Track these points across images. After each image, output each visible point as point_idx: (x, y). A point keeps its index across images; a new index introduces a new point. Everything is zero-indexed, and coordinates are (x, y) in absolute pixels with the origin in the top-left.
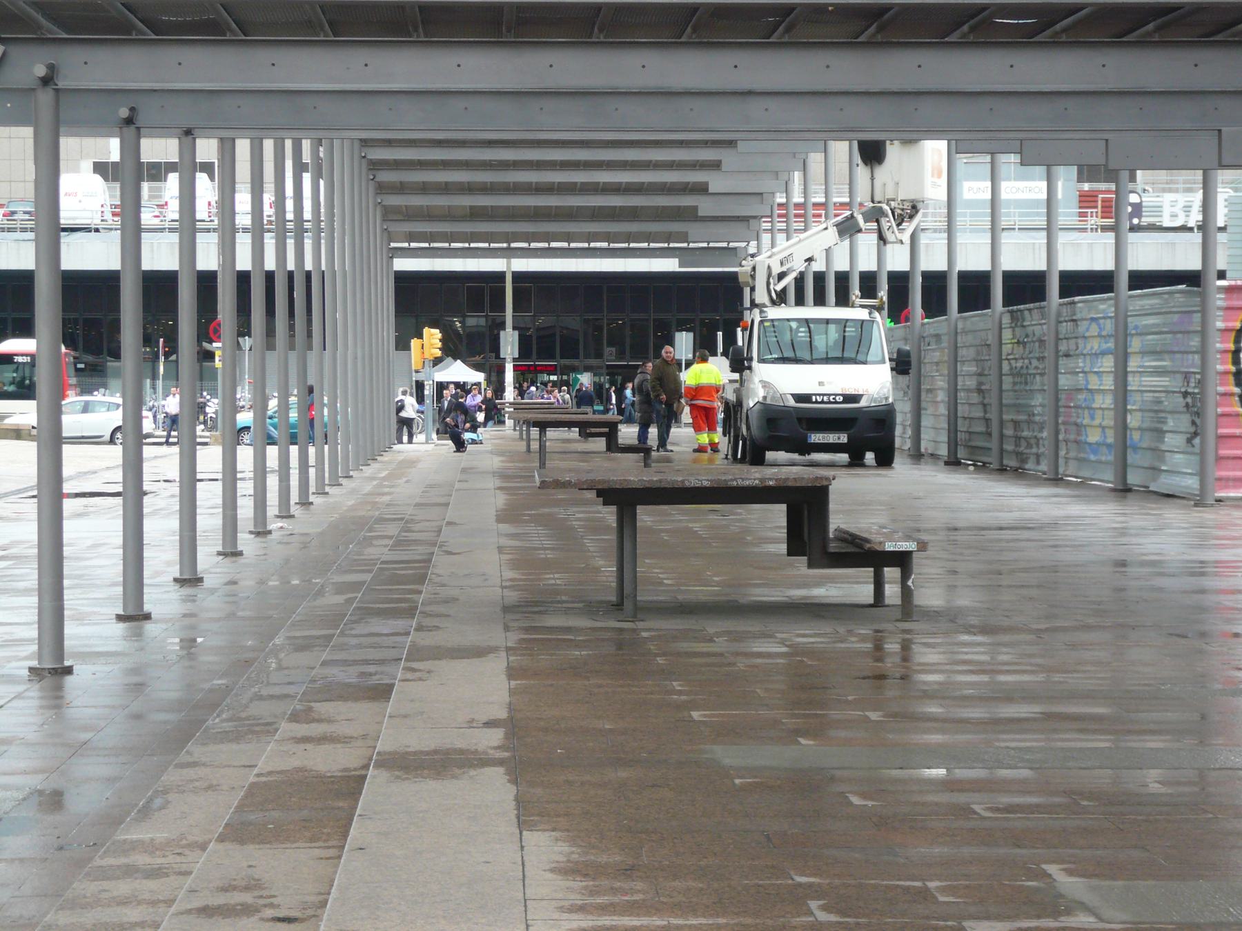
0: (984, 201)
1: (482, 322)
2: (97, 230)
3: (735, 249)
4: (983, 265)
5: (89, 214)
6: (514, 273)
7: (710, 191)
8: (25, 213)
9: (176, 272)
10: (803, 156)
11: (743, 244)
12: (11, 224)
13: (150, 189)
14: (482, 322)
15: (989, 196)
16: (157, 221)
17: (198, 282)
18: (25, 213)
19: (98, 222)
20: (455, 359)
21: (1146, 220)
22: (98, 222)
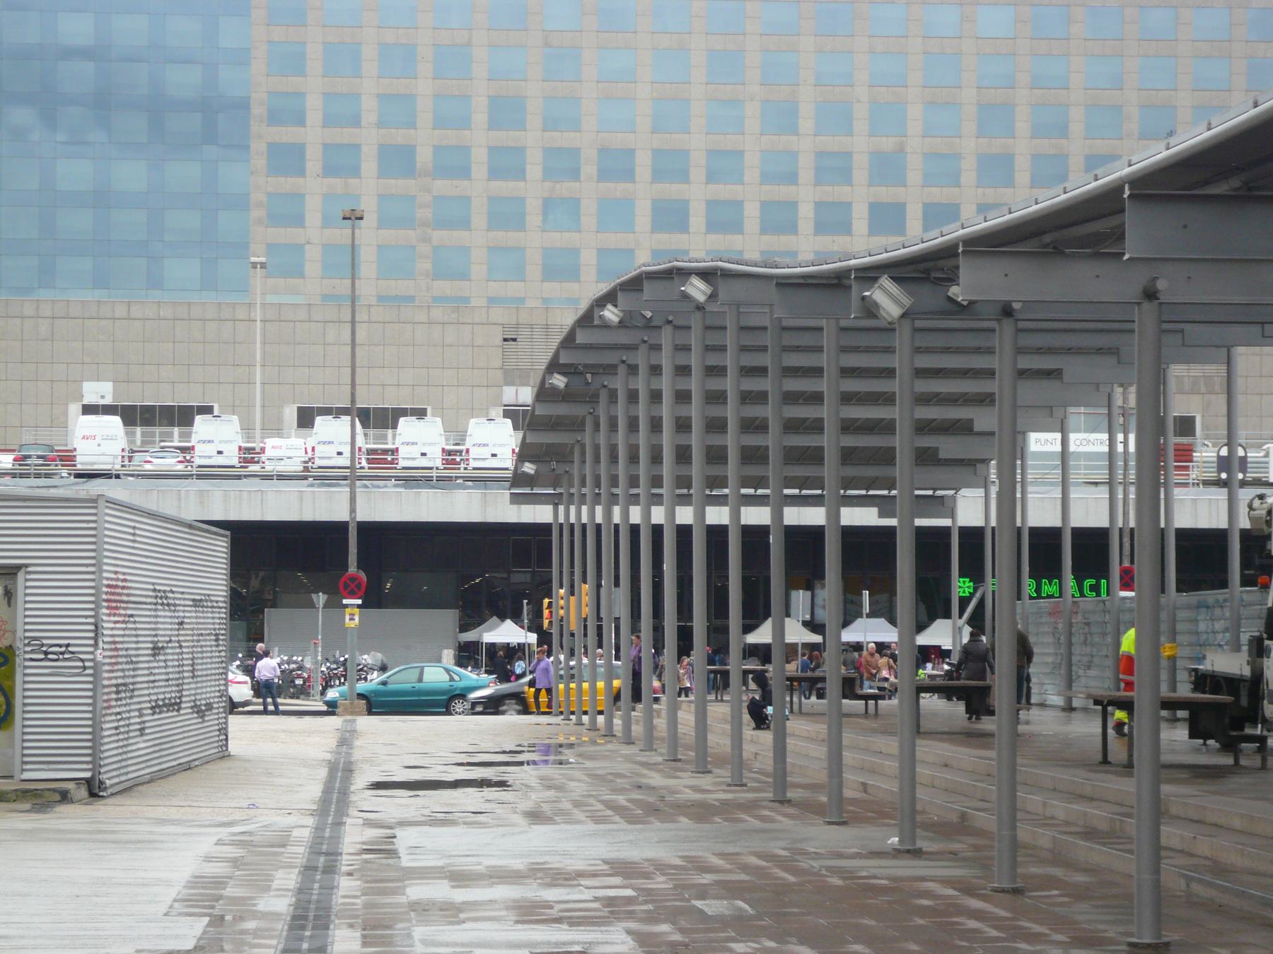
0: (1103, 453)
1: (528, 578)
2: (118, 477)
3: (942, 497)
4: (1101, 521)
5: (110, 459)
6: (961, 529)
7: (976, 429)
8: (39, 457)
9: (726, 526)
10: (1108, 390)
11: (952, 492)
12: (24, 470)
13: (143, 434)
14: (528, 578)
15: (1106, 449)
16: (180, 467)
17: (743, 537)
18: (39, 457)
19: (118, 467)
20: (502, 618)
21: (1250, 476)
22: (118, 467)
